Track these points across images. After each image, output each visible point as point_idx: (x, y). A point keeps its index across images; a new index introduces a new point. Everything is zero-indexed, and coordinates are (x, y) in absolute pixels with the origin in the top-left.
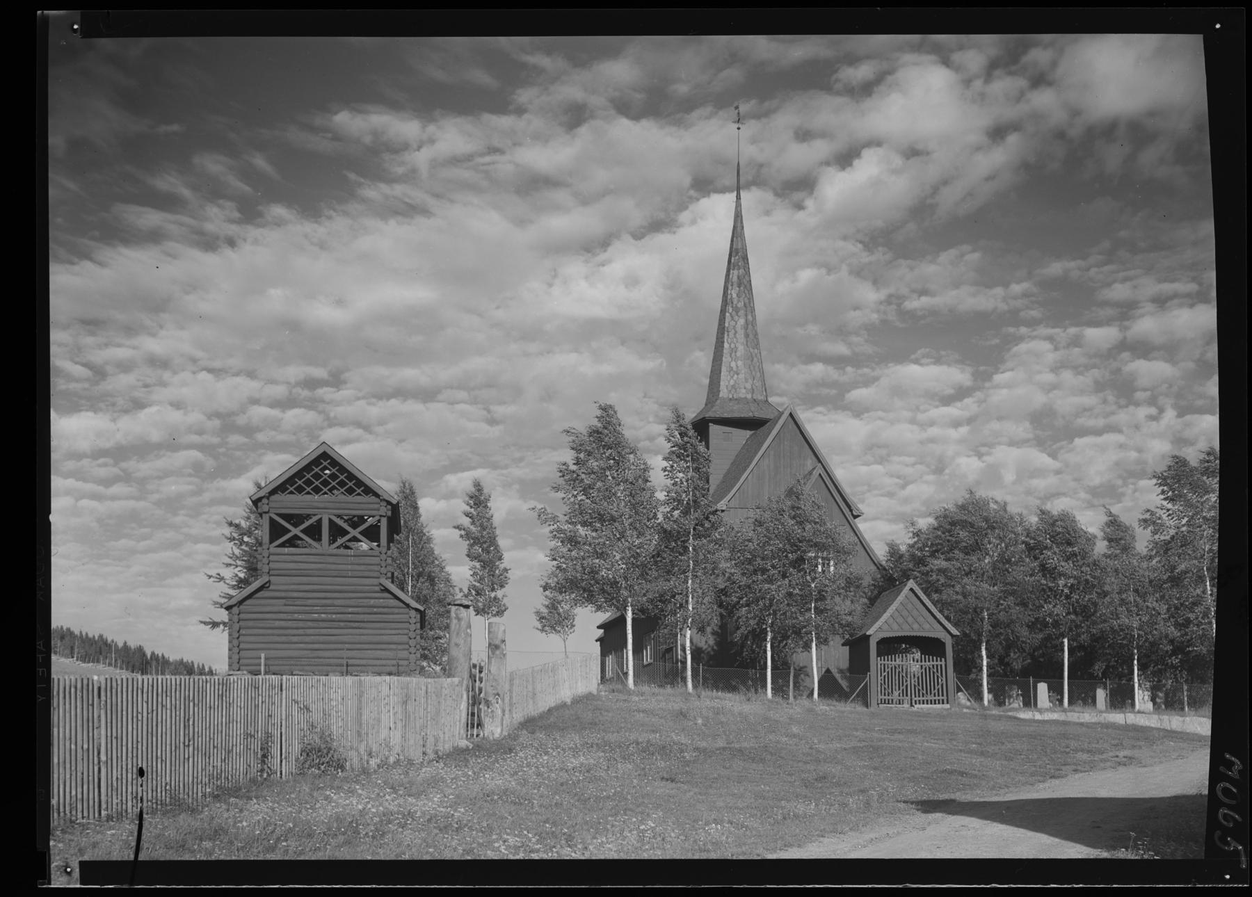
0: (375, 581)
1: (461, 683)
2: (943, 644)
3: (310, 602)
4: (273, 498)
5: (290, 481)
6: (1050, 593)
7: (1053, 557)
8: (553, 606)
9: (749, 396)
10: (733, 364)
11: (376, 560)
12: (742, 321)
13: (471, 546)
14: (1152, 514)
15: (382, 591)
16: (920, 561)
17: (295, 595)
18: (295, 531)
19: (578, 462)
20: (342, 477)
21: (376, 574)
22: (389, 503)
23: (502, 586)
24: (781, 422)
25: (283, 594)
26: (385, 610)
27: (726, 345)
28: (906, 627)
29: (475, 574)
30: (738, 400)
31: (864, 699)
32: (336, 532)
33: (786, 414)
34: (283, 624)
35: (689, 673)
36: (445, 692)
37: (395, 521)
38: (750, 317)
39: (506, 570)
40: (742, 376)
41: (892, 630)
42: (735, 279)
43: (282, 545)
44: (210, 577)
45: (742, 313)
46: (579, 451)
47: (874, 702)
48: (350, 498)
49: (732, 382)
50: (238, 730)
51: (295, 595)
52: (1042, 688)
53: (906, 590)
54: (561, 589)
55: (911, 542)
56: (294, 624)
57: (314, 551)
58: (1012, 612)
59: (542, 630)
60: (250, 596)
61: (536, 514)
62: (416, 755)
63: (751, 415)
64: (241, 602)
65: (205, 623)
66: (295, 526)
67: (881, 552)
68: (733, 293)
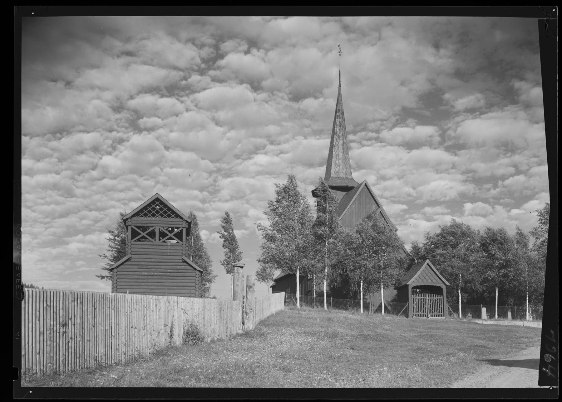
0: (181, 258)
1: (239, 303)
2: (442, 289)
3: (150, 267)
4: (134, 218)
5: (141, 211)
6: (489, 267)
7: (494, 249)
8: (264, 270)
9: (344, 176)
10: (337, 162)
11: (181, 248)
12: (341, 142)
13: (225, 241)
14: (536, 230)
15: (183, 262)
16: (432, 250)
17: (143, 263)
18: (143, 234)
19: (278, 201)
20: (165, 209)
21: (181, 254)
22: (187, 221)
23: (239, 261)
24: (361, 188)
25: (138, 263)
26: (185, 271)
27: (334, 153)
28: (425, 281)
29: (227, 255)
30: (339, 178)
31: (406, 314)
32: (163, 235)
33: (364, 184)
34: (137, 277)
35: (325, 301)
36: (234, 307)
37: (187, 229)
38: (345, 141)
39: (241, 253)
40: (341, 167)
41: (419, 282)
42: (338, 123)
43: (138, 240)
44: (100, 256)
45: (341, 138)
46: (279, 196)
47: (410, 315)
48: (169, 219)
49: (337, 170)
50: (162, 322)
51: (143, 263)
52: (484, 310)
53: (425, 264)
54: (264, 261)
55: (425, 242)
56: (143, 277)
57: (151, 243)
58: (472, 276)
59: (259, 280)
60: (122, 264)
61: (256, 226)
62: (223, 336)
63: (346, 185)
64: (118, 267)
65: (98, 277)
66: (143, 232)
67: (408, 248)
68: (337, 129)
